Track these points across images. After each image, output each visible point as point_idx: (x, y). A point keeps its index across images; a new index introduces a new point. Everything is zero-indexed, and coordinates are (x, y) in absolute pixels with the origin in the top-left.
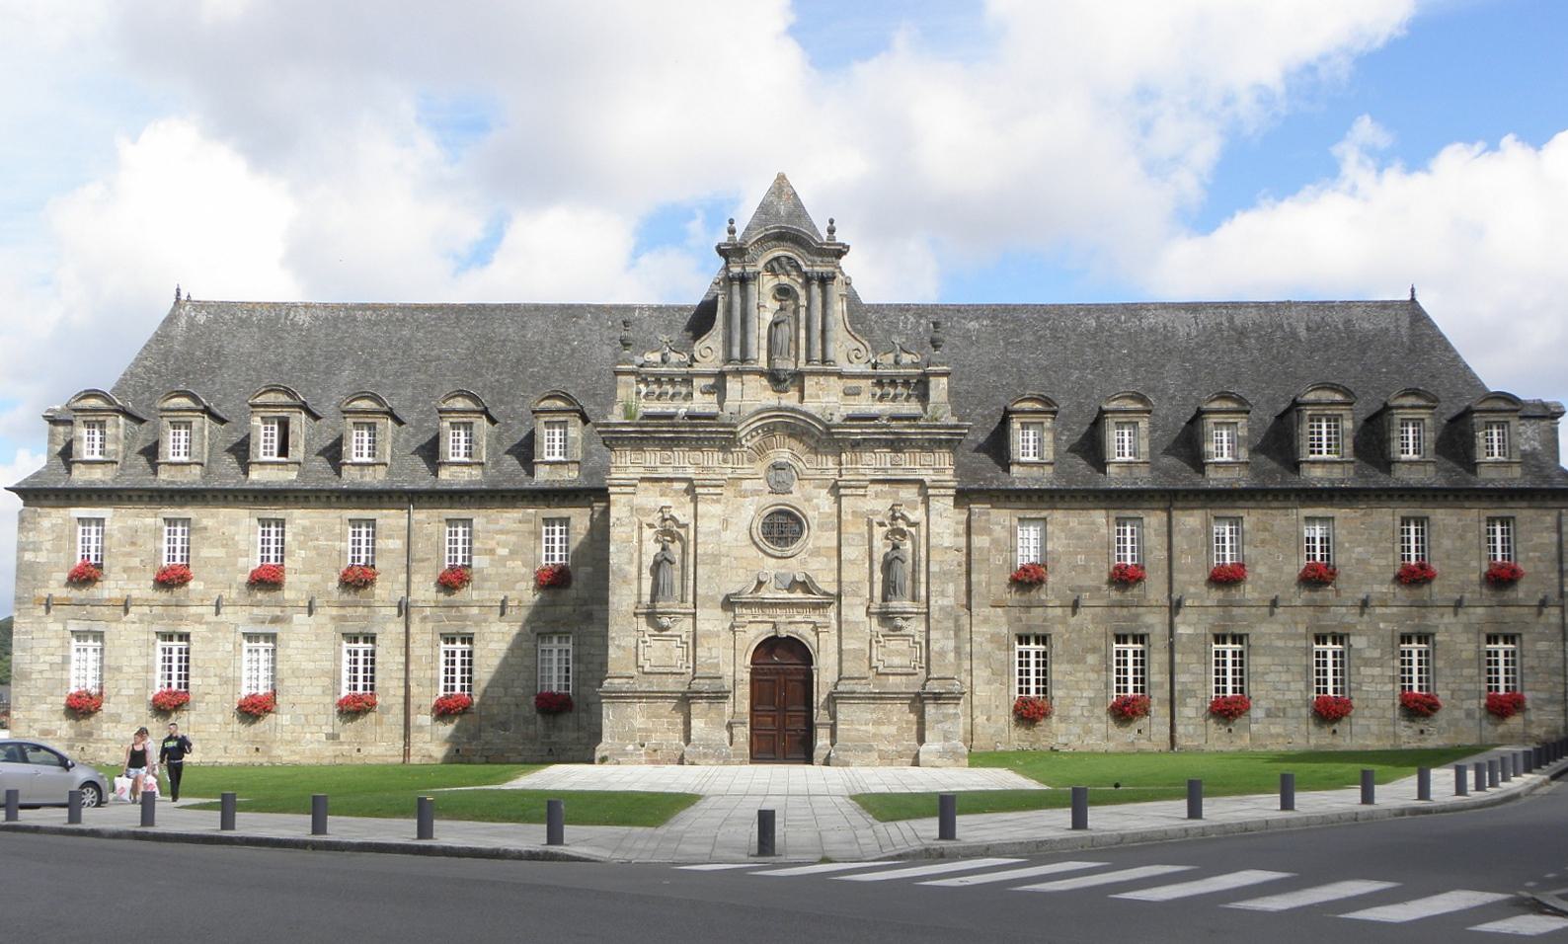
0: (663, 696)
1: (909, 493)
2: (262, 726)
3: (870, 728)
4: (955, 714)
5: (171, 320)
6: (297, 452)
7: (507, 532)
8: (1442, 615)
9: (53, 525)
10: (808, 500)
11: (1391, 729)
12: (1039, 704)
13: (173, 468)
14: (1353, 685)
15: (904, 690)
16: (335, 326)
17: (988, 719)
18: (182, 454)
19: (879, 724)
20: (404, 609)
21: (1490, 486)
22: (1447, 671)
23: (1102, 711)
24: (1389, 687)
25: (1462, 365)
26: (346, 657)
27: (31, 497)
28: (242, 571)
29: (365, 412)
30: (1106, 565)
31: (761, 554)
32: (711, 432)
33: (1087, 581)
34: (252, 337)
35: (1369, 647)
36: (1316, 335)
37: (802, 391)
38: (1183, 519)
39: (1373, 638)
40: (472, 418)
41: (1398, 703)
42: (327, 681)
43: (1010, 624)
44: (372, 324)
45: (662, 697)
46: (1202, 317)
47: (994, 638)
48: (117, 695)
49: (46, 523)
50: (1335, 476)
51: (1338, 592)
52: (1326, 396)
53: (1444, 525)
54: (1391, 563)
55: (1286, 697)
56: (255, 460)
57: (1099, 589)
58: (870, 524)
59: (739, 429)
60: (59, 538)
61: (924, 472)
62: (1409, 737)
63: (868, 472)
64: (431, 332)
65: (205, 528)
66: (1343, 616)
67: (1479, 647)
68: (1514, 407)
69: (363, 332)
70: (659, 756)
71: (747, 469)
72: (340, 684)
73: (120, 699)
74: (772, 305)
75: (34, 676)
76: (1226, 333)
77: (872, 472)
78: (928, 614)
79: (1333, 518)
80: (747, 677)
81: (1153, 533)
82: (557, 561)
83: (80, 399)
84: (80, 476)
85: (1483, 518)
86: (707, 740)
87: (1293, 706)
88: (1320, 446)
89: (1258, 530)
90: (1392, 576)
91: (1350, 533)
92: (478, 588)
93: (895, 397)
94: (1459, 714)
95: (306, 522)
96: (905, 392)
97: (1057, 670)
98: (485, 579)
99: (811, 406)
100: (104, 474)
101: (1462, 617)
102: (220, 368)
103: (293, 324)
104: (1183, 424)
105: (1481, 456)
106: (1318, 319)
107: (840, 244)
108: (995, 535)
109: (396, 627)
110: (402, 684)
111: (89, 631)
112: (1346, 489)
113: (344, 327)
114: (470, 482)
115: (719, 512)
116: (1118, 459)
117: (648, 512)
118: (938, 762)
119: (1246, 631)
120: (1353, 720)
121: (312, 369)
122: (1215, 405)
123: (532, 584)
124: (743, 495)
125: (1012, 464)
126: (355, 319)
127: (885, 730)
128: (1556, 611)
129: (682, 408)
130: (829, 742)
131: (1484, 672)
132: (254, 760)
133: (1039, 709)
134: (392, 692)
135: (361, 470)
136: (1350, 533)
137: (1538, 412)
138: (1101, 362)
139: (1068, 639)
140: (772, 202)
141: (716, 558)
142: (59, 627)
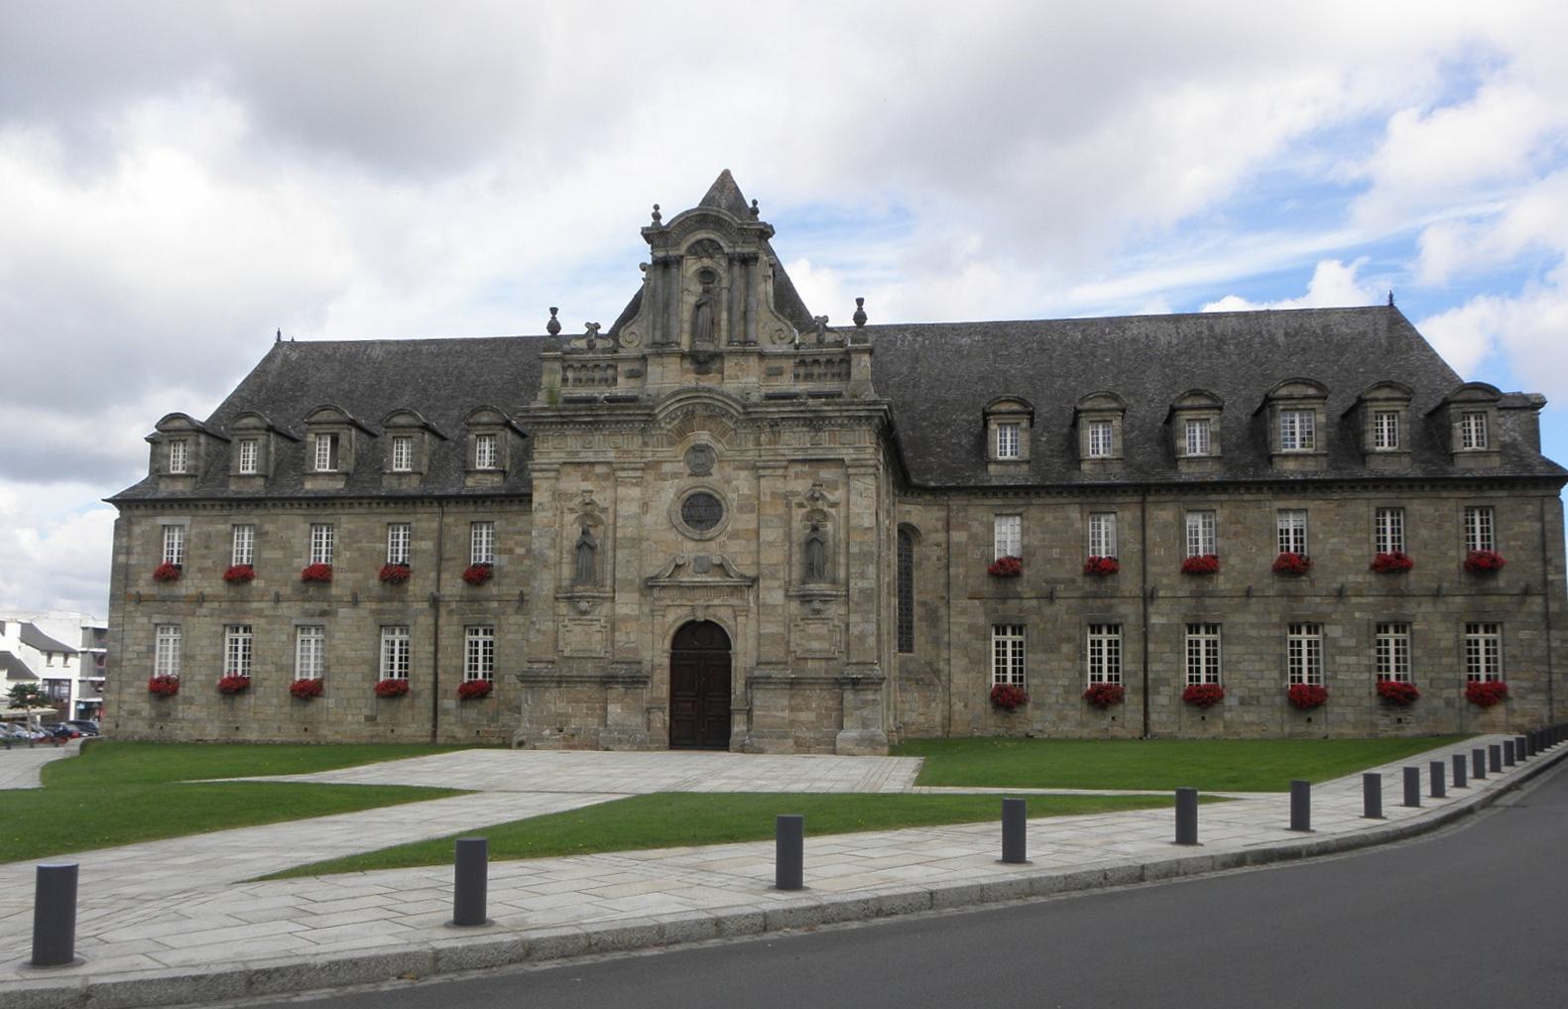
0: (582, 680)
1: (826, 474)
2: (311, 708)
4: (874, 700)
5: (268, 359)
8: (1419, 605)
10: (728, 482)
11: (1367, 717)
12: (1015, 691)
15: (824, 675)
16: (403, 360)
17: (966, 706)
20: (435, 602)
21: (1468, 475)
22: (1426, 660)
23: (1076, 699)
24: (1365, 676)
25: (1440, 363)
28: (297, 570)
31: (680, 538)
32: (629, 415)
33: (1063, 574)
35: (1344, 636)
36: (1294, 340)
38: (1156, 512)
39: (1348, 627)
40: (496, 430)
41: (1374, 691)
42: (366, 668)
43: (987, 615)
45: (581, 682)
46: (1184, 327)
47: (972, 629)
50: (1307, 469)
51: (1312, 582)
52: (1298, 390)
53: (1421, 515)
54: (1367, 553)
55: (1260, 686)
57: (1073, 581)
58: (788, 505)
59: (656, 411)
61: (845, 451)
63: (787, 452)
65: (267, 533)
66: (1319, 604)
67: (1458, 636)
71: (666, 452)
72: (378, 671)
74: (697, 288)
75: (124, 663)
76: (1206, 341)
78: (847, 596)
79: (1306, 510)
80: (666, 662)
81: (1126, 527)
83: (166, 423)
84: (165, 489)
85: (1461, 507)
87: (1267, 695)
89: (1231, 523)
90: (1367, 567)
91: (1324, 524)
92: (499, 584)
94: (1439, 703)
95: (351, 526)
97: (1031, 659)
99: (731, 387)
101: (1442, 607)
102: (302, 396)
104: (1160, 424)
105: (1458, 446)
106: (1297, 325)
107: (761, 223)
108: (973, 530)
109: (425, 621)
110: (431, 671)
112: (1319, 481)
114: (492, 488)
116: (1092, 456)
117: (570, 497)
118: (856, 750)
119: (1219, 621)
120: (1328, 708)
122: (1188, 403)
124: (663, 477)
127: (804, 716)
128: (1539, 600)
129: (601, 392)
130: (745, 728)
132: (303, 739)
133: (1013, 696)
134: (422, 678)
135: (400, 479)
137: (1518, 404)
138: (1084, 370)
139: (1043, 629)
140: (714, 197)
141: (636, 542)
142: (145, 620)
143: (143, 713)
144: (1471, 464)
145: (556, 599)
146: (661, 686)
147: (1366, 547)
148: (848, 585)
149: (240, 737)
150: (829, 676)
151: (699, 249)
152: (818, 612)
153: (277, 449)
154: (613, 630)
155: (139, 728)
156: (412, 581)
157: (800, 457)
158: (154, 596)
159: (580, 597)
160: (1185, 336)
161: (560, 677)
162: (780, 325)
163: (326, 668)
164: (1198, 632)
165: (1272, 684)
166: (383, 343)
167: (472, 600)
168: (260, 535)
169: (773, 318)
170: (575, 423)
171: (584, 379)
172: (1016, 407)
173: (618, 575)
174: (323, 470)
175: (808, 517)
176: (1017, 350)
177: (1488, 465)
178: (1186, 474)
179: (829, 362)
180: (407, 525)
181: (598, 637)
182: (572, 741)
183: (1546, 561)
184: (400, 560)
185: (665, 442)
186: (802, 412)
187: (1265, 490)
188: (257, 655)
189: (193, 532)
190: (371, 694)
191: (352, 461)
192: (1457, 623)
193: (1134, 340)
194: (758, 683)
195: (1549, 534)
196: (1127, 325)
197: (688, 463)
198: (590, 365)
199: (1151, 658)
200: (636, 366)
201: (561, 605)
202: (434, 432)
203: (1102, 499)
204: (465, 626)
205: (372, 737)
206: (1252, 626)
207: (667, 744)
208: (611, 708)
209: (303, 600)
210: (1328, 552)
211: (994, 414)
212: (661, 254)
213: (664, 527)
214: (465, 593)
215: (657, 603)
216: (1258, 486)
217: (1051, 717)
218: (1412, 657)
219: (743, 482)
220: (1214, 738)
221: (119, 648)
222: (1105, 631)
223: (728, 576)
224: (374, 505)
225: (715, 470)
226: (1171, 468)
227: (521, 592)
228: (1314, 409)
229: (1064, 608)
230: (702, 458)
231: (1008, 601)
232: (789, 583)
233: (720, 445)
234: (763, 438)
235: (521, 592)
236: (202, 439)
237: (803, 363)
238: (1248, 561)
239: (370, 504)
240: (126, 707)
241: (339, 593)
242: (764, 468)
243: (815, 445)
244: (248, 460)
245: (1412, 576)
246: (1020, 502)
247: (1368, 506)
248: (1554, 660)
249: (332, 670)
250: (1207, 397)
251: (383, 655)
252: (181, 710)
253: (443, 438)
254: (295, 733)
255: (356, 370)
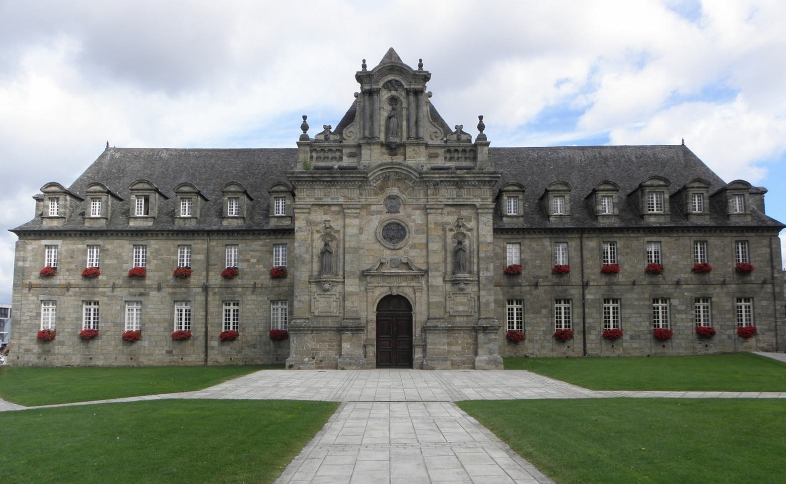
0: (326, 329)
1: (465, 212)
2: (134, 347)
3: (446, 347)
4: (495, 339)
5: (103, 156)
6: (154, 213)
7: (256, 251)
8: (715, 289)
9: (33, 249)
10: (409, 216)
11: (692, 344)
12: (519, 333)
13: (92, 220)
14: (673, 323)
18: (97, 214)
19: (451, 345)
20: (206, 288)
21: (737, 225)
22: (718, 316)
23: (549, 337)
24: (690, 324)
26: (176, 312)
27: (22, 234)
28: (125, 271)
29: (186, 192)
30: (550, 266)
31: (382, 248)
33: (541, 273)
34: (140, 164)
37: (405, 155)
39: (681, 300)
40: (239, 195)
41: (694, 331)
42: (166, 325)
43: (504, 295)
44: (196, 157)
45: (325, 330)
48: (63, 332)
49: (29, 247)
51: (664, 278)
54: (689, 263)
55: (640, 329)
56: (132, 216)
57: (547, 277)
58: (444, 230)
59: (369, 176)
60: (36, 255)
61: (476, 200)
62: (700, 348)
63: (443, 200)
64: (224, 161)
67: (733, 304)
68: (747, 187)
69: (193, 161)
70: (323, 364)
71: (373, 199)
72: (173, 326)
73: (64, 333)
74: (388, 108)
75: (22, 323)
76: (598, 160)
77: (445, 200)
78: (479, 281)
79: (660, 242)
80: (375, 318)
82: (281, 265)
83: (47, 187)
84: (46, 225)
85: (733, 241)
86: (352, 355)
87: (643, 334)
88: (653, 207)
90: (690, 270)
91: (669, 249)
92: (242, 279)
93: (458, 158)
94: (725, 337)
95: (157, 246)
96: (463, 156)
97: (528, 317)
98: (245, 274)
99: (410, 162)
100: (58, 223)
101: (725, 290)
102: (123, 177)
103: (160, 157)
105: (731, 212)
107: (426, 72)
109: (201, 298)
110: (204, 326)
111: (49, 300)
113: (184, 159)
114: (238, 226)
115: (358, 223)
116: (555, 214)
120: (673, 340)
121: (167, 177)
122: (602, 187)
123: (268, 276)
124: (372, 213)
125: (504, 216)
126: (189, 155)
127: (454, 348)
128: (770, 286)
130: (421, 355)
131: (736, 316)
132: (129, 364)
134: (198, 330)
136: (669, 249)
141: (356, 250)
142: (35, 298)
143: (34, 351)
144: (737, 220)
145: (310, 282)
146: (372, 333)
147: (689, 260)
148: (478, 274)
149: (92, 363)
150: (469, 325)
151: (390, 85)
152: (462, 289)
153: (112, 204)
154: (344, 301)
155: (32, 359)
156: (192, 277)
157: (451, 203)
158: (40, 285)
159: (324, 281)
160: (588, 157)
161: (313, 327)
162: (435, 130)
163: (143, 324)
164: (560, 303)
165: (646, 328)
166: (167, 150)
167: (227, 287)
168: (103, 250)
169: (431, 125)
170: (320, 181)
171: (322, 157)
172: (516, 188)
173: (347, 269)
174: (141, 216)
175: (455, 237)
176: (506, 162)
177: (745, 220)
178: (603, 223)
179: (464, 151)
180: (189, 246)
181: (334, 304)
182: (321, 365)
183: (773, 267)
184: (185, 265)
185: (372, 193)
186: (453, 177)
187: (641, 231)
188: (102, 317)
189: (63, 249)
190: (170, 339)
191: (156, 210)
192: (733, 298)
193: (563, 158)
194: (430, 330)
195: (774, 254)
196: (559, 151)
197: (386, 205)
198: (326, 149)
199: (587, 316)
200: (353, 150)
201: (313, 286)
202: (202, 197)
203: (561, 236)
204: (223, 301)
205: (170, 362)
206: (636, 300)
207: (375, 366)
208: (344, 345)
209: (130, 287)
210: (671, 263)
211: (505, 191)
212: (367, 87)
213: (372, 242)
214: (223, 283)
215: (369, 285)
216: (638, 230)
217: (537, 346)
218: (712, 315)
219: (417, 217)
220: (618, 356)
221: (19, 314)
222: (563, 302)
223: (411, 269)
224: (170, 235)
225: (401, 209)
226: (594, 220)
227: (255, 283)
228: (663, 192)
229: (543, 291)
230: (394, 203)
231: (515, 287)
232: (445, 273)
233: (404, 196)
234: (429, 191)
235: (255, 283)
236: (68, 198)
237: (449, 151)
238: (632, 265)
239: (168, 234)
240: (23, 347)
241: (150, 283)
242: (431, 209)
243: (459, 196)
244: (95, 210)
245: (712, 274)
246: (520, 237)
247: (690, 240)
248: (778, 316)
249: (146, 326)
250: (612, 185)
251: (176, 317)
252: (57, 349)
253: (206, 200)
254: (125, 360)
255: (153, 163)
